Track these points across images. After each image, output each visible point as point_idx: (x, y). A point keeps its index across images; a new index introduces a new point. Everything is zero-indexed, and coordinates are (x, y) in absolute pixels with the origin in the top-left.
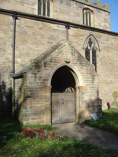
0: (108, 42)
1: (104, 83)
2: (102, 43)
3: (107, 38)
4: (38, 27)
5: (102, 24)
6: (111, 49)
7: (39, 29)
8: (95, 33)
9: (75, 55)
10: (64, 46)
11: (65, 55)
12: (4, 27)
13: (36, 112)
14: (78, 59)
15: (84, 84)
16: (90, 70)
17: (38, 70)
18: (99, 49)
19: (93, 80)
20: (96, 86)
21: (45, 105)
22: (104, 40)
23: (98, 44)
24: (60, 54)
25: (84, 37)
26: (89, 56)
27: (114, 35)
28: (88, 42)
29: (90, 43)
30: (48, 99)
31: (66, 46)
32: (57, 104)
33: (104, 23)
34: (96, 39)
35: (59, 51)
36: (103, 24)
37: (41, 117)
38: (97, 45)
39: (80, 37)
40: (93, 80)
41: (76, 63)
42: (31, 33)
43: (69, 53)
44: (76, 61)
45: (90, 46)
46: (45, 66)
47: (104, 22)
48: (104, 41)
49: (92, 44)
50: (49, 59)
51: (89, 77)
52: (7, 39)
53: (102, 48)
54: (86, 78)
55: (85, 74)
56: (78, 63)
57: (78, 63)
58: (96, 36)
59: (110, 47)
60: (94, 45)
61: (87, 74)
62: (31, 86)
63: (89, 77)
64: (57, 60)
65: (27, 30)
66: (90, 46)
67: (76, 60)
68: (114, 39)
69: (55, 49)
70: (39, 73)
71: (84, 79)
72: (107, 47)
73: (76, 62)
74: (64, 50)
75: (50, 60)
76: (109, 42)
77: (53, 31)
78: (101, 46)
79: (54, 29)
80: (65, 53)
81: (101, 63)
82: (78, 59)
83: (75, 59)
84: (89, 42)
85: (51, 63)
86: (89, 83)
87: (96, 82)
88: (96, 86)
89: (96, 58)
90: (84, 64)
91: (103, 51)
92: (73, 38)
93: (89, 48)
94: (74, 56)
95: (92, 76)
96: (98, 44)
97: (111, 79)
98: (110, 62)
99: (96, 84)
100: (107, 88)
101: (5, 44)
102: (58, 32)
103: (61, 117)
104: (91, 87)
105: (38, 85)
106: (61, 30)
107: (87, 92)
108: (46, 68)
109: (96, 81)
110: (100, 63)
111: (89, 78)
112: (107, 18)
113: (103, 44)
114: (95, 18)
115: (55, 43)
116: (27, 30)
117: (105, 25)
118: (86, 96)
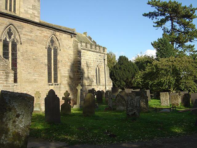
0: (31, 34)
1: (25, 82)
2: (24, 35)
3: (30, 29)
5: (29, 12)
6: (36, 43)
8: (16, 23)
16: (3, 66)
18: (21, 41)
19: (7, 78)
22: (27, 31)
23: (19, 36)
25: (2, 27)
26: (8, 50)
27: (40, 26)
28: (6, 32)
29: (10, 34)
33: (31, 10)
34: (17, 30)
36: (31, 11)
38: (19, 37)
40: (7, 78)
45: (10, 37)
47: (32, 9)
49: (12, 35)
51: (2, 74)
53: (24, 41)
56: (52, 75)
59: (34, 40)
60: (15, 37)
63: (2, 74)
66: (10, 37)
68: (39, 31)
72: (30, 40)
76: (33, 35)
78: (23, 38)
81: (23, 59)
84: (8, 32)
86: (2, 82)
88: (11, 85)
89: (17, 52)
91: (26, 44)
93: (8, 40)
96: (19, 36)
97: (35, 78)
98: (34, 57)
99: (10, 82)
100: (30, 88)
110: (21, 58)
112: (36, 5)
114: (22, 3)
117: (32, 13)
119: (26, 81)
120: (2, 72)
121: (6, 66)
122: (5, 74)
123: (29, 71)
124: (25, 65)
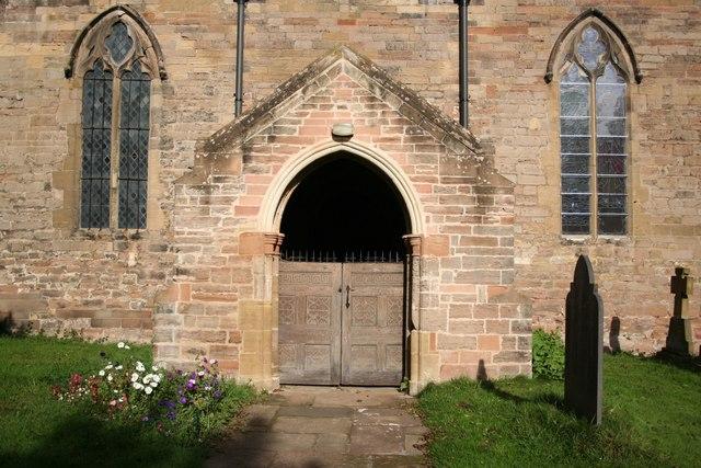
0: (691, 35)
2: (653, 43)
4: (336, 16)
7: (340, 22)
9: (384, 106)
10: (337, 70)
11: (335, 109)
12: (211, 36)
13: (205, 326)
14: (400, 121)
15: (432, 224)
17: (216, 173)
18: (636, 71)
20: (499, 237)
21: (242, 304)
22: (668, 28)
24: (314, 106)
25: (554, 30)
30: (253, 282)
31: (343, 73)
32: (320, 308)
35: (310, 94)
37: (225, 348)
39: (532, 31)
40: (480, 210)
41: (391, 140)
42: (308, 45)
43: (356, 100)
44: (392, 130)
46: (246, 159)
48: (666, 33)
50: (263, 132)
51: (458, 193)
52: (221, 74)
54: (442, 200)
55: (439, 185)
57: (398, 139)
58: (619, 15)
61: (445, 181)
62: (190, 233)
63: (458, 193)
64: (300, 133)
65: (292, 33)
67: (390, 125)
69: (293, 89)
70: (221, 185)
71: (431, 204)
72: (685, 59)
73: (387, 136)
74: (334, 90)
75: (267, 135)
77: (400, 22)
79: (406, 16)
80: (335, 100)
82: (400, 121)
83: (385, 122)
85: (272, 145)
86: (458, 224)
87: (499, 218)
88: (499, 237)
90: (430, 138)
92: (497, 38)
94: (379, 111)
95: (477, 190)
99: (495, 224)
101: (211, 94)
102: (424, 25)
103: (337, 359)
104: (465, 240)
105: (214, 230)
106: (438, 15)
107: (446, 263)
108: (251, 165)
109: (496, 216)
111: (457, 199)
113: (664, 47)
115: (297, 67)
116: (292, 33)
118: (439, 278)
119: (667, 228)
120: (458, 186)
121: (476, 162)
122: (475, 195)
123: (683, 187)
124: (658, 161)
